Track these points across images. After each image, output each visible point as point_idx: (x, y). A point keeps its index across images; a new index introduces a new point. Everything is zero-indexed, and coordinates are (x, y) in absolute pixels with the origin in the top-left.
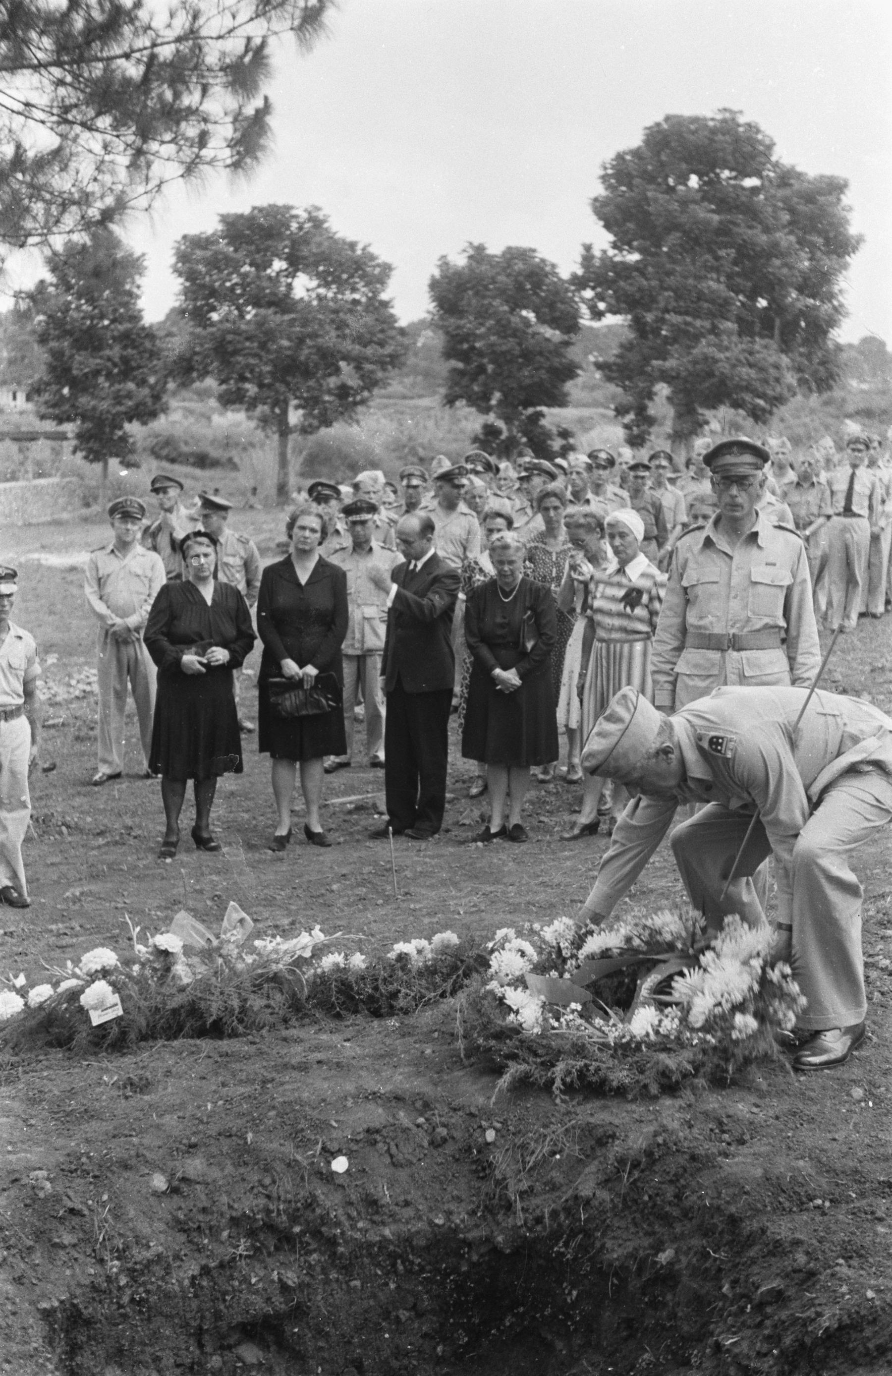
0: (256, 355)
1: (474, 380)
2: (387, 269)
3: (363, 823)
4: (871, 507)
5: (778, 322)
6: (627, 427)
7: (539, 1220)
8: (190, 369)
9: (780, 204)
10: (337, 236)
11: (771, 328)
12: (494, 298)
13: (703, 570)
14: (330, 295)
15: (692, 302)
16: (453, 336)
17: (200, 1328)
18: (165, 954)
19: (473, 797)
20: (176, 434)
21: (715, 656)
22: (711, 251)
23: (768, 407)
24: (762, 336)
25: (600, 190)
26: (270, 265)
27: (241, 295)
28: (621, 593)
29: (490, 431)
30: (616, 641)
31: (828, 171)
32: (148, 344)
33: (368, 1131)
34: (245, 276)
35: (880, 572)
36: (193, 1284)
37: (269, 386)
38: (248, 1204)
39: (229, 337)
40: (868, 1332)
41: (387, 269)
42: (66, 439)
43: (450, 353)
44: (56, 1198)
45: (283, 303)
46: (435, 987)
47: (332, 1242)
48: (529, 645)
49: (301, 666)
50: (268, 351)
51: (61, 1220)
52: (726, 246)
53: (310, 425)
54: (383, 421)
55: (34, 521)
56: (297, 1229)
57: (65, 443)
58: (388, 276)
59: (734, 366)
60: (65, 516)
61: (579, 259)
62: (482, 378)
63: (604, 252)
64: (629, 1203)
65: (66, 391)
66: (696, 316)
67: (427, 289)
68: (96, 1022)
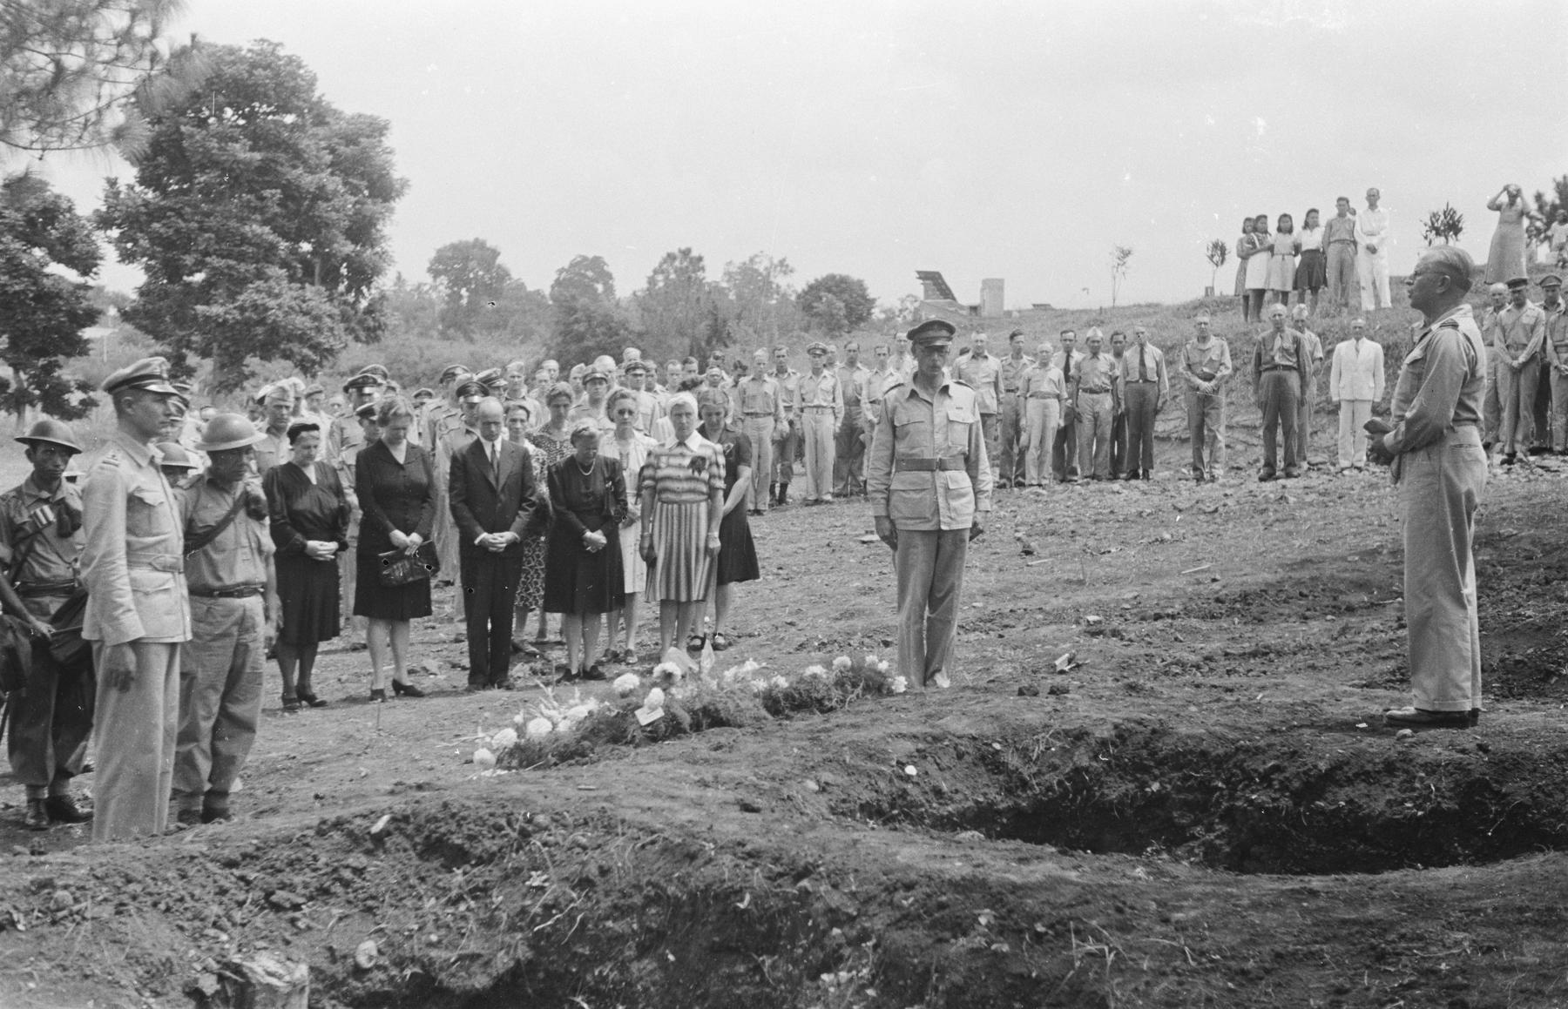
7: (1050, 789)
21: (927, 475)
23: (317, 358)
28: (687, 462)
30: (685, 502)
38: (867, 796)
49: (408, 534)
52: (270, 185)
59: (287, 314)
61: (102, 195)
63: (131, 187)
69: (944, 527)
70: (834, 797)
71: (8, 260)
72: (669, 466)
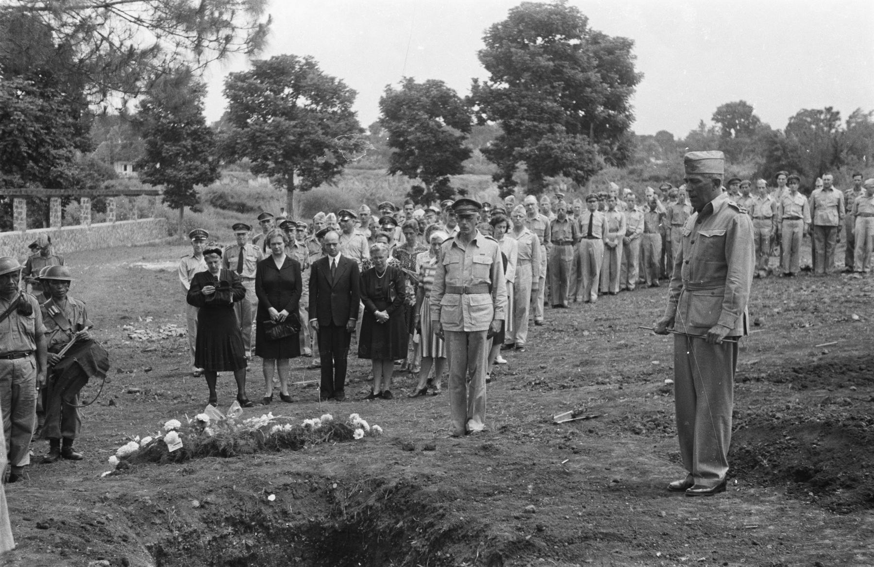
0: (273, 145)
1: (407, 159)
2: (353, 93)
3: (311, 392)
4: (603, 233)
5: (592, 125)
6: (500, 187)
7: (352, 517)
8: (234, 153)
9: (591, 55)
10: (323, 74)
11: (589, 129)
12: (419, 110)
13: (453, 257)
14: (319, 108)
15: (538, 114)
16: (394, 133)
17: (212, 562)
18: (202, 422)
19: (369, 381)
20: (226, 192)
21: (457, 296)
22: (551, 83)
24: (582, 133)
25: (483, 46)
26: (282, 91)
27: (264, 109)
29: (417, 190)
31: (621, 34)
32: (208, 138)
33: (284, 485)
34: (266, 97)
35: (616, 268)
36: (209, 544)
37: (282, 162)
38: (232, 513)
39: (258, 134)
40: (459, 531)
41: (353, 93)
42: (158, 194)
43: (392, 144)
44: (153, 506)
45: (291, 112)
46: (321, 437)
47: (268, 528)
48: (393, 299)
49: (279, 311)
50: (281, 143)
51: (155, 514)
53: (306, 185)
54: (356, 183)
55: (138, 244)
56: (253, 523)
57: (157, 197)
58: (354, 98)
59: (563, 152)
60: (157, 241)
61: (470, 87)
62: (411, 158)
64: (387, 508)
65: (158, 166)
66: (541, 122)
67: (378, 105)
68: (171, 450)
69: (466, 330)
70: (207, 512)
71: (422, 124)
72: (429, 275)
